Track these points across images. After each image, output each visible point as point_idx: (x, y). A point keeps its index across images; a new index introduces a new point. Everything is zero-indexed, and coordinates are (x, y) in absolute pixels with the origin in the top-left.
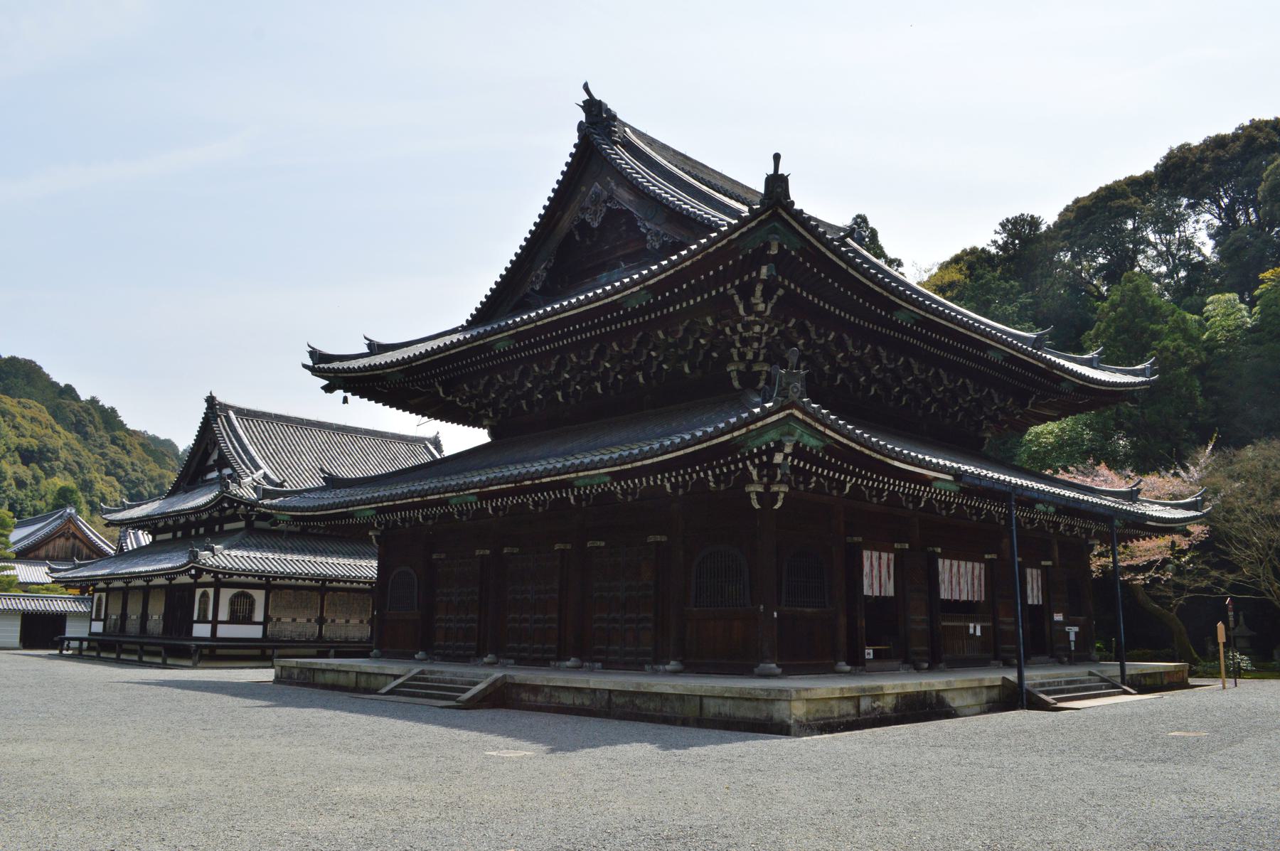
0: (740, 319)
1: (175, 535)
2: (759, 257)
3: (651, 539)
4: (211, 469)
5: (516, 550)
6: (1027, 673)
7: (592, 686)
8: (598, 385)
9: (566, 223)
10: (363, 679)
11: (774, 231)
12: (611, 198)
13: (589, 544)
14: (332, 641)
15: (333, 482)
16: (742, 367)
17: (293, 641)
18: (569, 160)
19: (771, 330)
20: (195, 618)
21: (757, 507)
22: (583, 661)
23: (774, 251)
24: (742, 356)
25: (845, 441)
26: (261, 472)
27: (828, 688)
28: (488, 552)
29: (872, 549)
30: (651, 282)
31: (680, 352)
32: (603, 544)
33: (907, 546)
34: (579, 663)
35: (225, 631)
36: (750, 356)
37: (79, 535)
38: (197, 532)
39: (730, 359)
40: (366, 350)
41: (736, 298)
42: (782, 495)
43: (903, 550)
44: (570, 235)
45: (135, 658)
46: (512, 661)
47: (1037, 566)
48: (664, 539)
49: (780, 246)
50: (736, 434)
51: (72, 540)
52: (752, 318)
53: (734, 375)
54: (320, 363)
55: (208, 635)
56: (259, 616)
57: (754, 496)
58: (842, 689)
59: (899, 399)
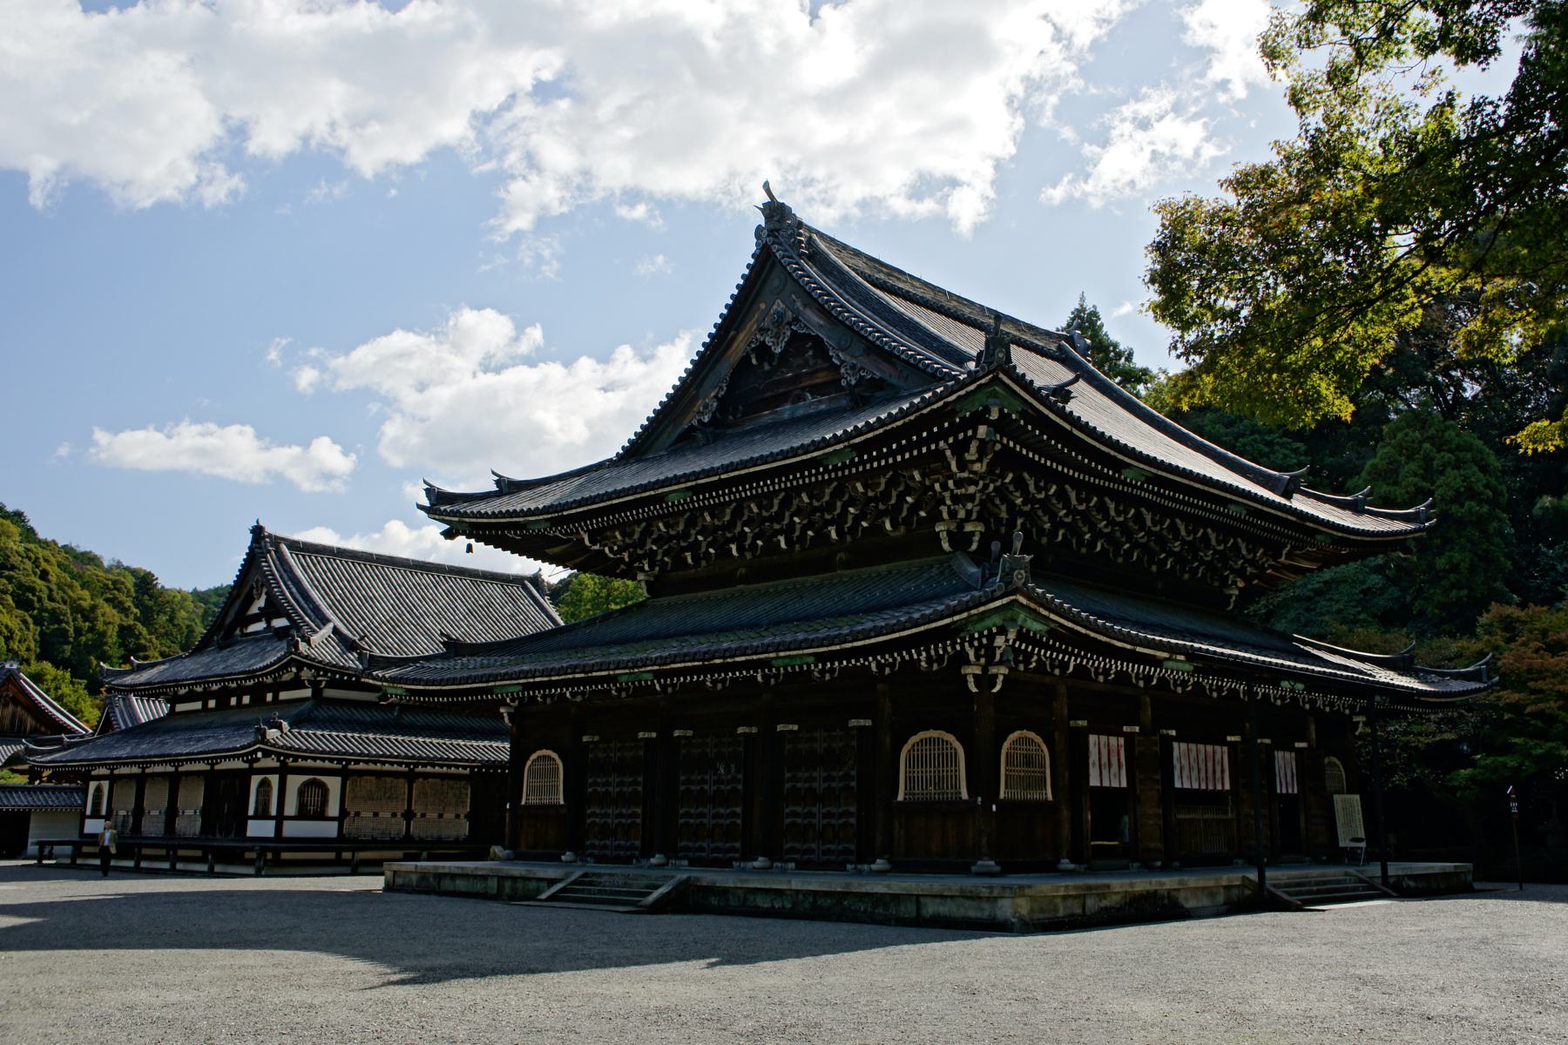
0: (952, 476)
1: (205, 704)
2: (980, 418)
3: (853, 723)
4: (256, 619)
5: (690, 733)
6: (1268, 874)
7: (794, 887)
8: (782, 539)
9: (741, 343)
10: (520, 885)
11: (995, 395)
12: (796, 320)
13: (780, 728)
14: (422, 841)
15: (454, 648)
16: (953, 527)
17: (374, 840)
18: (747, 272)
19: (986, 486)
20: (251, 812)
21: (974, 690)
22: (772, 860)
23: (994, 415)
24: (953, 514)
25: (1070, 625)
26: (331, 625)
27: (1051, 888)
28: (654, 735)
29: (1099, 733)
30: (857, 440)
31: (881, 507)
32: (796, 728)
33: (1137, 729)
34: (768, 864)
35: (292, 829)
36: (962, 514)
37: (21, 697)
38: (239, 700)
39: (940, 519)
40: (494, 488)
41: (948, 453)
42: (1001, 678)
43: (1132, 734)
44: (746, 359)
45: (166, 865)
46: (685, 862)
47: (1291, 749)
48: (868, 723)
49: (1001, 411)
50: (956, 618)
51: (11, 707)
52: (965, 475)
53: (943, 535)
54: (440, 504)
55: (272, 835)
56: (333, 809)
57: (971, 679)
58: (1067, 887)
59: (1129, 553)
